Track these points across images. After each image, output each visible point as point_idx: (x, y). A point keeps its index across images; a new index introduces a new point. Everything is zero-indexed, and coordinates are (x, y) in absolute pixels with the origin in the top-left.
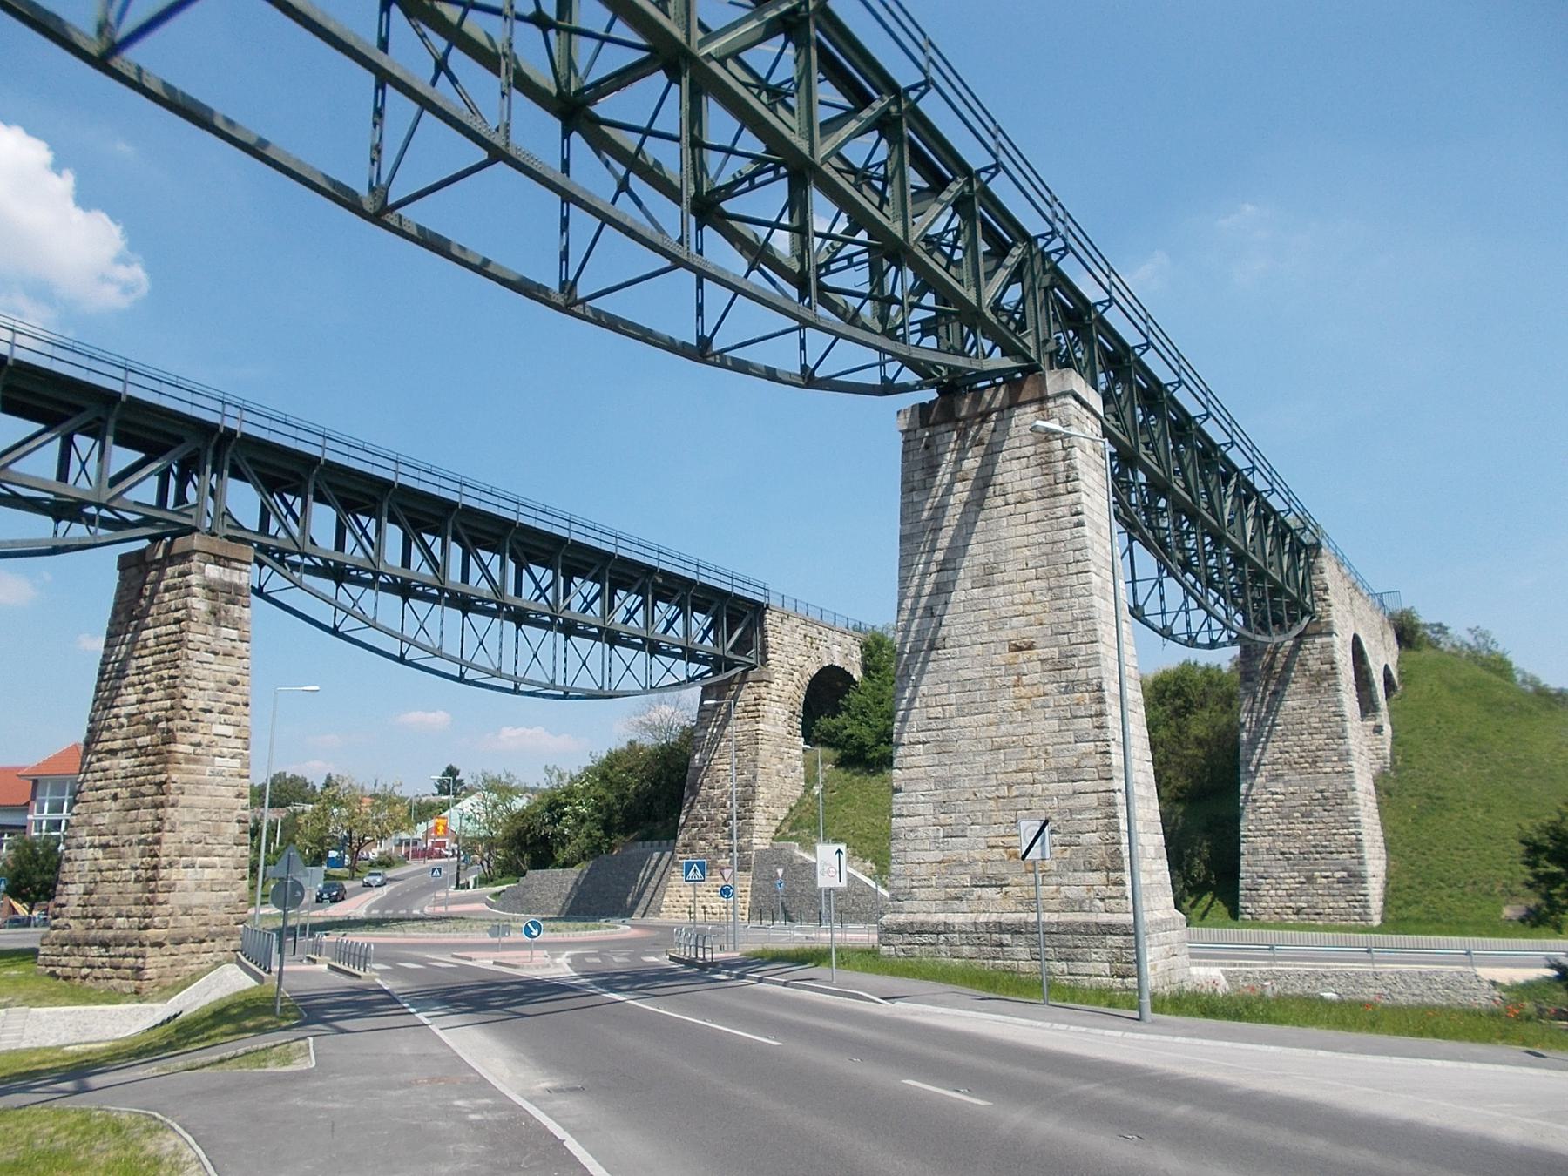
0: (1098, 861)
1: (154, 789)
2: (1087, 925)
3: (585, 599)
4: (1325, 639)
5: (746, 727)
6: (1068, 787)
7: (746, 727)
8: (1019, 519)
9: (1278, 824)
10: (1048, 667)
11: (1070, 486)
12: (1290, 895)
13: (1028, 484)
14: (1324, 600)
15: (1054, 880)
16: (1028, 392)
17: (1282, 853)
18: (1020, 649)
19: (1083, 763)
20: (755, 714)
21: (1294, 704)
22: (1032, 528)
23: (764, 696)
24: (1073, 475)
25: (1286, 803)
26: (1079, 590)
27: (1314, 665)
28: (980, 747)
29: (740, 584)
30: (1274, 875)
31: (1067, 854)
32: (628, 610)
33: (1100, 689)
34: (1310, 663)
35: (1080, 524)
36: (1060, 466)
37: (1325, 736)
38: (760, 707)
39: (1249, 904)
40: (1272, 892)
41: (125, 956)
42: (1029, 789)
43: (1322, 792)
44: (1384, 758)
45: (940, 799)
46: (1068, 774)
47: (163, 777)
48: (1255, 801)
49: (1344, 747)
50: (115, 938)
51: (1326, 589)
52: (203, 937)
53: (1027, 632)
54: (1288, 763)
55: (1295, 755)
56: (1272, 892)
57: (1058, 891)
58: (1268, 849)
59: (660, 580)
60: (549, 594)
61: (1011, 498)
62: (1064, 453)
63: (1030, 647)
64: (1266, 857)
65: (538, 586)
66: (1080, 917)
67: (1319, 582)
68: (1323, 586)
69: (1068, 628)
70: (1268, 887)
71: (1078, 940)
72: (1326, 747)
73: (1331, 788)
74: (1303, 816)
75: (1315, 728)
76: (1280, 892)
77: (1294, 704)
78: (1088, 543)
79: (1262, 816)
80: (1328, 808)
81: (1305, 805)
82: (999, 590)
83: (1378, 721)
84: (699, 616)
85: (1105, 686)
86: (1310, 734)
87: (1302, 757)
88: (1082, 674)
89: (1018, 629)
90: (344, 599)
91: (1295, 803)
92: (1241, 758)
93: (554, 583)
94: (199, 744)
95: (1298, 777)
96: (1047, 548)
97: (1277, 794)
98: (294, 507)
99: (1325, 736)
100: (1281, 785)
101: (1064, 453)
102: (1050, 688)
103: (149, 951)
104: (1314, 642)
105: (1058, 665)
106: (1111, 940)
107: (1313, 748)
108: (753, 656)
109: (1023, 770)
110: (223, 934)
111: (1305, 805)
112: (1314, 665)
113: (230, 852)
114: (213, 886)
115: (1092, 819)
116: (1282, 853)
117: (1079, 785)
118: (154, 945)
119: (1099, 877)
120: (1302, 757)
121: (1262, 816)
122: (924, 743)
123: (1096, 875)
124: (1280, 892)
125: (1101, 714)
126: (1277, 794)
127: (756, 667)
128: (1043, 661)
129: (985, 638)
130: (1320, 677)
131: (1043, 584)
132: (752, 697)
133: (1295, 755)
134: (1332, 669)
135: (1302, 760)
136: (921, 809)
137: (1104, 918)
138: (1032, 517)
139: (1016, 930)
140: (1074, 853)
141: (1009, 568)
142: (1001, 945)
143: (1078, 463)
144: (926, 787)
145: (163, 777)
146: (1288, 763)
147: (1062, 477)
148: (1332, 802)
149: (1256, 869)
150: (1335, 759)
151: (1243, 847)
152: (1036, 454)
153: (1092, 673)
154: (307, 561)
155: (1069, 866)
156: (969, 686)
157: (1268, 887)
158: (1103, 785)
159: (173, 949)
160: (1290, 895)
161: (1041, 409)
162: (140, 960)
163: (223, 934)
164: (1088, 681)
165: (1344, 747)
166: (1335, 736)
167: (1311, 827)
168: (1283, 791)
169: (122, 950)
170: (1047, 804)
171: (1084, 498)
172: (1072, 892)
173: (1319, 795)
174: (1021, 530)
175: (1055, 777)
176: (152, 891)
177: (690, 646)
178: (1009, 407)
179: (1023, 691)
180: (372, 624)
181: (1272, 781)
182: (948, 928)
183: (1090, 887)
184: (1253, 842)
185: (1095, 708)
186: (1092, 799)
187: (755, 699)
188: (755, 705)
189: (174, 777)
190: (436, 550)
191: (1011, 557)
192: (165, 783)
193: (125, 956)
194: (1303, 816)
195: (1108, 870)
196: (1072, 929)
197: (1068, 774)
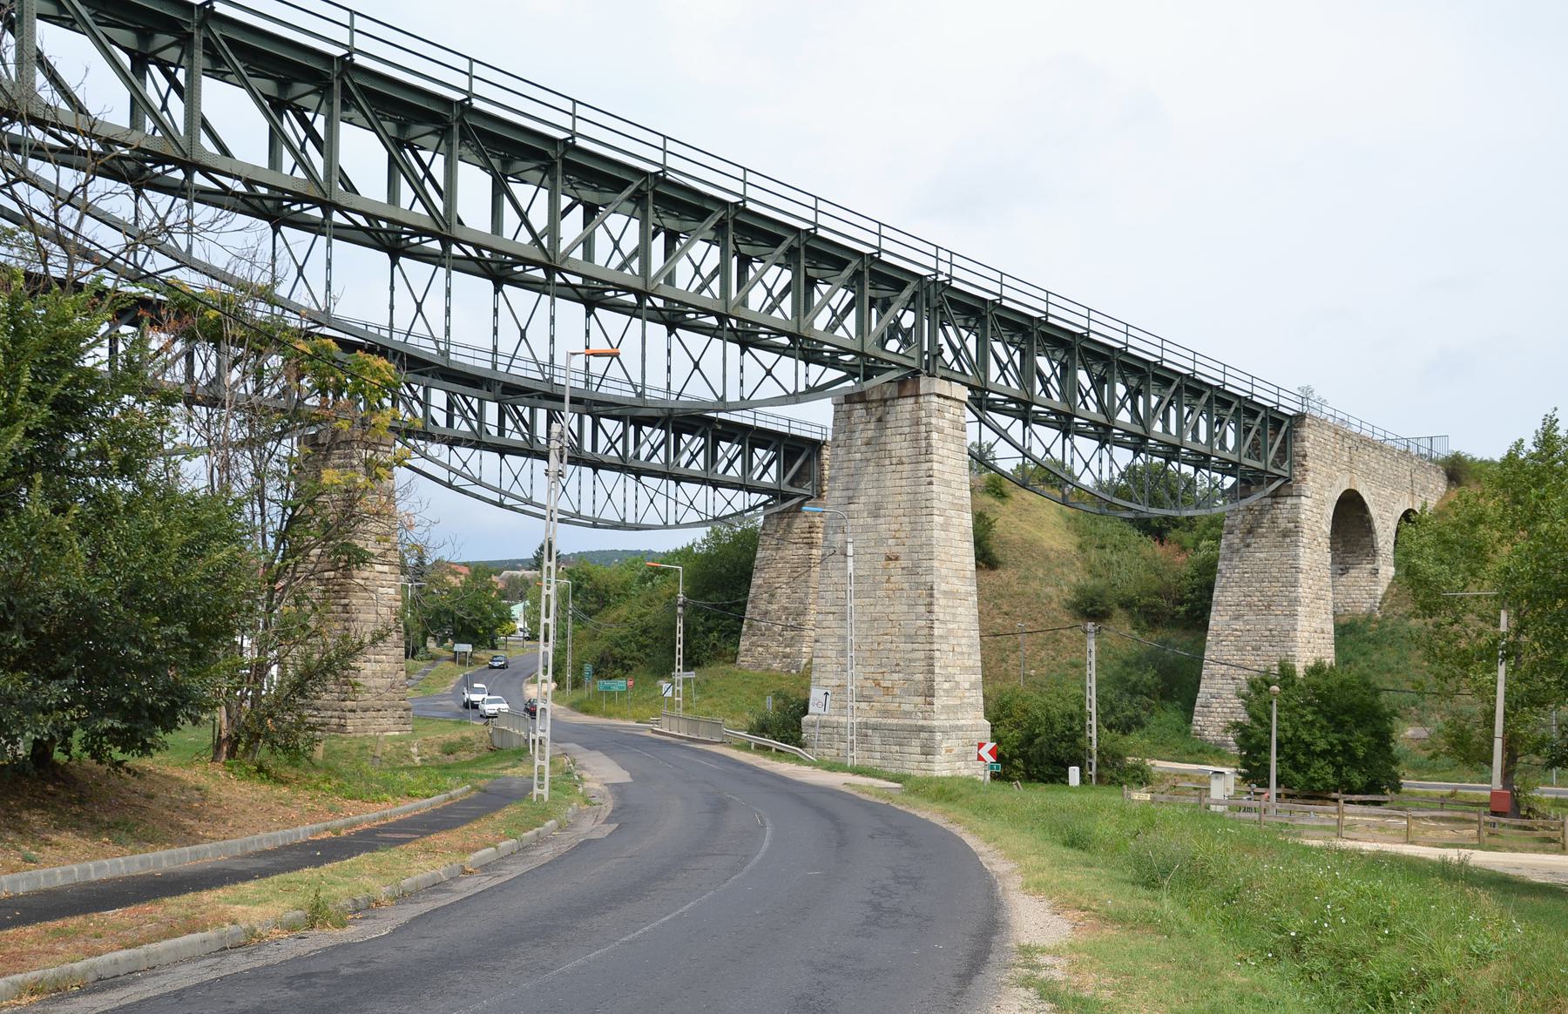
0: (921, 691)
1: (340, 608)
2: (911, 726)
3: (652, 446)
4: (1295, 501)
5: (801, 552)
6: (910, 646)
7: (801, 552)
8: (898, 475)
9: (1234, 655)
10: (905, 572)
11: (928, 457)
12: (1233, 712)
13: (904, 452)
14: (1303, 465)
15: (898, 700)
16: (909, 389)
17: (1233, 679)
18: (891, 559)
19: (919, 633)
20: (809, 541)
21: (1261, 555)
22: (904, 482)
23: (818, 524)
24: (930, 449)
25: (1243, 639)
26: (926, 526)
27: (1283, 524)
28: (865, 618)
29: (798, 425)
30: (1224, 696)
31: (906, 686)
32: (692, 453)
33: (932, 589)
34: (1280, 521)
35: (931, 483)
36: (923, 443)
37: (1280, 584)
38: (813, 535)
39: (1200, 718)
40: (1219, 710)
41: (331, 717)
42: (889, 646)
43: (1271, 630)
44: (1375, 598)
45: (840, 648)
46: (911, 639)
47: (346, 601)
48: (1218, 635)
49: (1294, 594)
50: (323, 706)
51: (1305, 456)
52: (379, 708)
53: (895, 549)
54: (1249, 605)
55: (1256, 599)
56: (1219, 710)
57: (899, 706)
58: (1223, 675)
59: (720, 427)
60: (619, 446)
61: (894, 462)
62: (926, 434)
63: (897, 559)
64: (1220, 681)
65: (610, 439)
66: (908, 722)
67: (1300, 449)
68: (1302, 453)
69: (918, 549)
70: (1217, 705)
71: (906, 734)
72: (1280, 594)
73: (1279, 628)
74: (1253, 650)
75: (1274, 577)
76: (1225, 710)
77: (1261, 555)
78: (934, 495)
79: (1222, 648)
80: (1273, 644)
81: (1256, 641)
82: (882, 520)
83: (1375, 566)
84: (760, 452)
85: (935, 587)
86: (1270, 582)
87: (1260, 601)
88: (923, 579)
89: (891, 546)
90: (456, 464)
91: (1249, 639)
92: (1214, 599)
93: (624, 435)
94: (367, 579)
95: (1254, 618)
96: (911, 497)
97: (1236, 630)
98: (315, 125)
99: (1280, 584)
100: (1241, 623)
101: (926, 434)
102: (906, 586)
103: (348, 714)
104: (1285, 503)
105: (911, 571)
106: (922, 735)
107: (1270, 594)
108: (810, 488)
109: (887, 634)
110: (393, 707)
111: (1256, 641)
112: (1283, 524)
113: (392, 652)
114: (383, 674)
115: (920, 666)
116: (1233, 679)
117: (916, 646)
118: (350, 711)
119: (920, 700)
120: (1260, 601)
121: (1222, 648)
122: (834, 613)
123: (920, 698)
124: (1225, 710)
125: (931, 604)
126: (1236, 630)
127: (812, 497)
128: (903, 568)
129: (873, 550)
130: (1285, 534)
131: (907, 519)
132: (807, 525)
133: (1256, 599)
134: (1296, 527)
135: (1260, 603)
136: (829, 653)
137: (921, 722)
138: (905, 475)
139: (875, 728)
140: (910, 685)
141: (890, 506)
142: (866, 736)
143: (934, 443)
144: (833, 640)
145: (346, 601)
146: (1249, 605)
147: (923, 451)
148: (1277, 639)
149: (1211, 690)
150: (1285, 604)
151: (1204, 672)
152: (910, 433)
153: (928, 578)
154: (337, 217)
155: (907, 692)
156: (861, 579)
157: (1217, 705)
158: (927, 647)
159: (362, 714)
160: (1233, 712)
161: (916, 403)
162: (343, 721)
163: (393, 707)
164: (925, 583)
165: (1294, 594)
166: (1288, 585)
167: (1258, 658)
168: (1242, 628)
169: (329, 713)
170: (898, 656)
171: (935, 466)
172: (905, 707)
173: (1268, 633)
174: (898, 483)
175: (903, 640)
176: (346, 677)
177: (747, 483)
178: (898, 398)
179: (891, 586)
180: (478, 482)
181: (1235, 619)
182: (838, 725)
183: (916, 705)
184: (1212, 669)
185: (928, 599)
186: (921, 655)
187: (810, 527)
188: (810, 532)
189: (354, 601)
190: (526, 415)
191: (891, 499)
192: (347, 605)
193: (331, 717)
194: (1253, 650)
195: (926, 696)
196: (903, 728)
197: (911, 639)
